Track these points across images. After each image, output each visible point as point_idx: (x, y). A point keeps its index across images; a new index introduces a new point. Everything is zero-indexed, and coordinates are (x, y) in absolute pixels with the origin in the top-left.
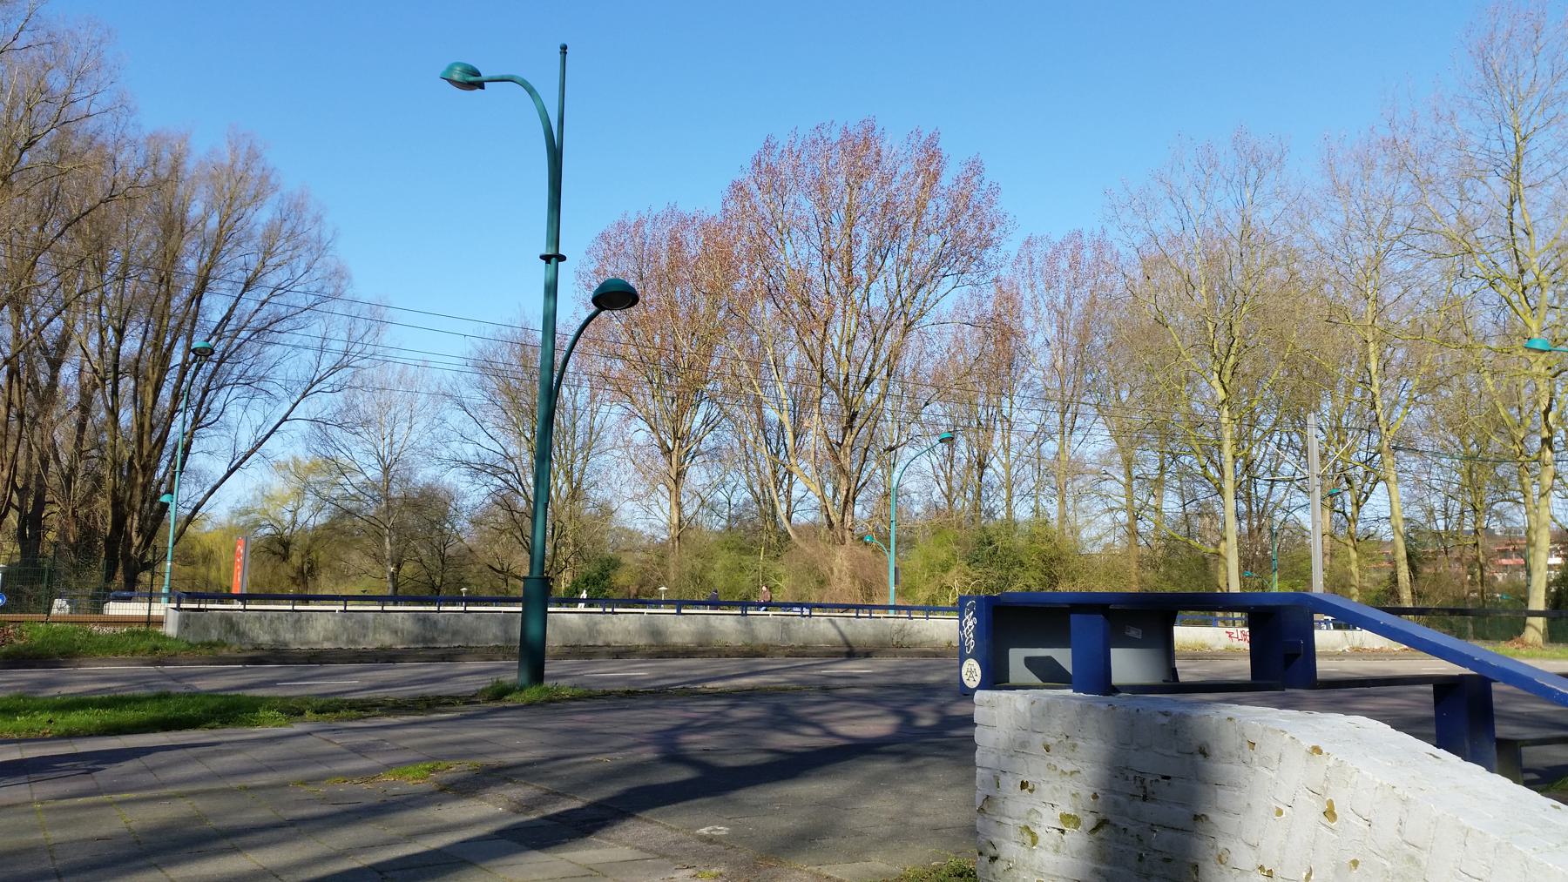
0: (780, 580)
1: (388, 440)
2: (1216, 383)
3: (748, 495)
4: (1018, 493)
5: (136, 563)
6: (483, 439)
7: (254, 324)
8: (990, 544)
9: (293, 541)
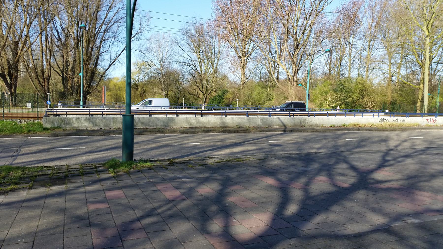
0: (274, 97)
1: (161, 56)
2: (425, 29)
3: (266, 71)
4: (353, 68)
5: (85, 92)
6: (185, 55)
7: (113, 20)
8: (342, 85)
9: (139, 84)
